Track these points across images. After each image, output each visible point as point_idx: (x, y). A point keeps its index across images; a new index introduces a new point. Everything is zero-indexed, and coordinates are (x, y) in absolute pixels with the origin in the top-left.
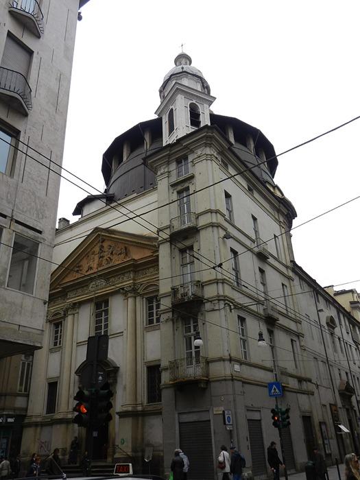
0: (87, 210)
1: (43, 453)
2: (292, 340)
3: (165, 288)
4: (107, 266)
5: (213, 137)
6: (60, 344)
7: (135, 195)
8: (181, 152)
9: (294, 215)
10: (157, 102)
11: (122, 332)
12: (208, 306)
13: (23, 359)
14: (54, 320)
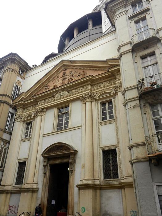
6: (29, 136)
11: (81, 126)
13: (2, 144)
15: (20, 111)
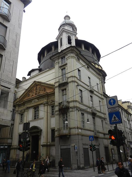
0: (33, 74)
1: (17, 158)
2: (102, 121)
3: (56, 104)
4: (39, 94)
5: (74, 50)
7: (48, 69)
8: (63, 55)
9: (106, 75)
10: (57, 33)
12: (71, 110)
14: (21, 113)
15: (17, 109)
